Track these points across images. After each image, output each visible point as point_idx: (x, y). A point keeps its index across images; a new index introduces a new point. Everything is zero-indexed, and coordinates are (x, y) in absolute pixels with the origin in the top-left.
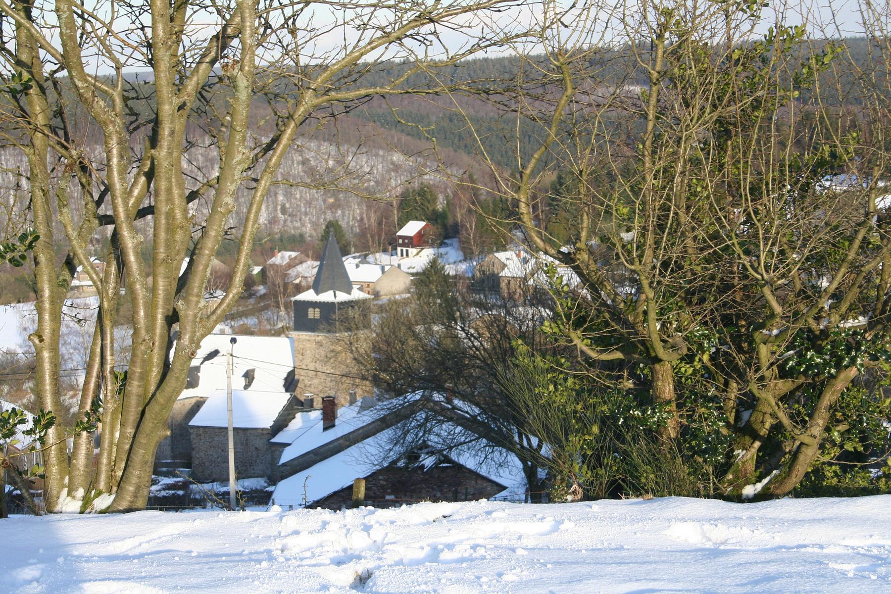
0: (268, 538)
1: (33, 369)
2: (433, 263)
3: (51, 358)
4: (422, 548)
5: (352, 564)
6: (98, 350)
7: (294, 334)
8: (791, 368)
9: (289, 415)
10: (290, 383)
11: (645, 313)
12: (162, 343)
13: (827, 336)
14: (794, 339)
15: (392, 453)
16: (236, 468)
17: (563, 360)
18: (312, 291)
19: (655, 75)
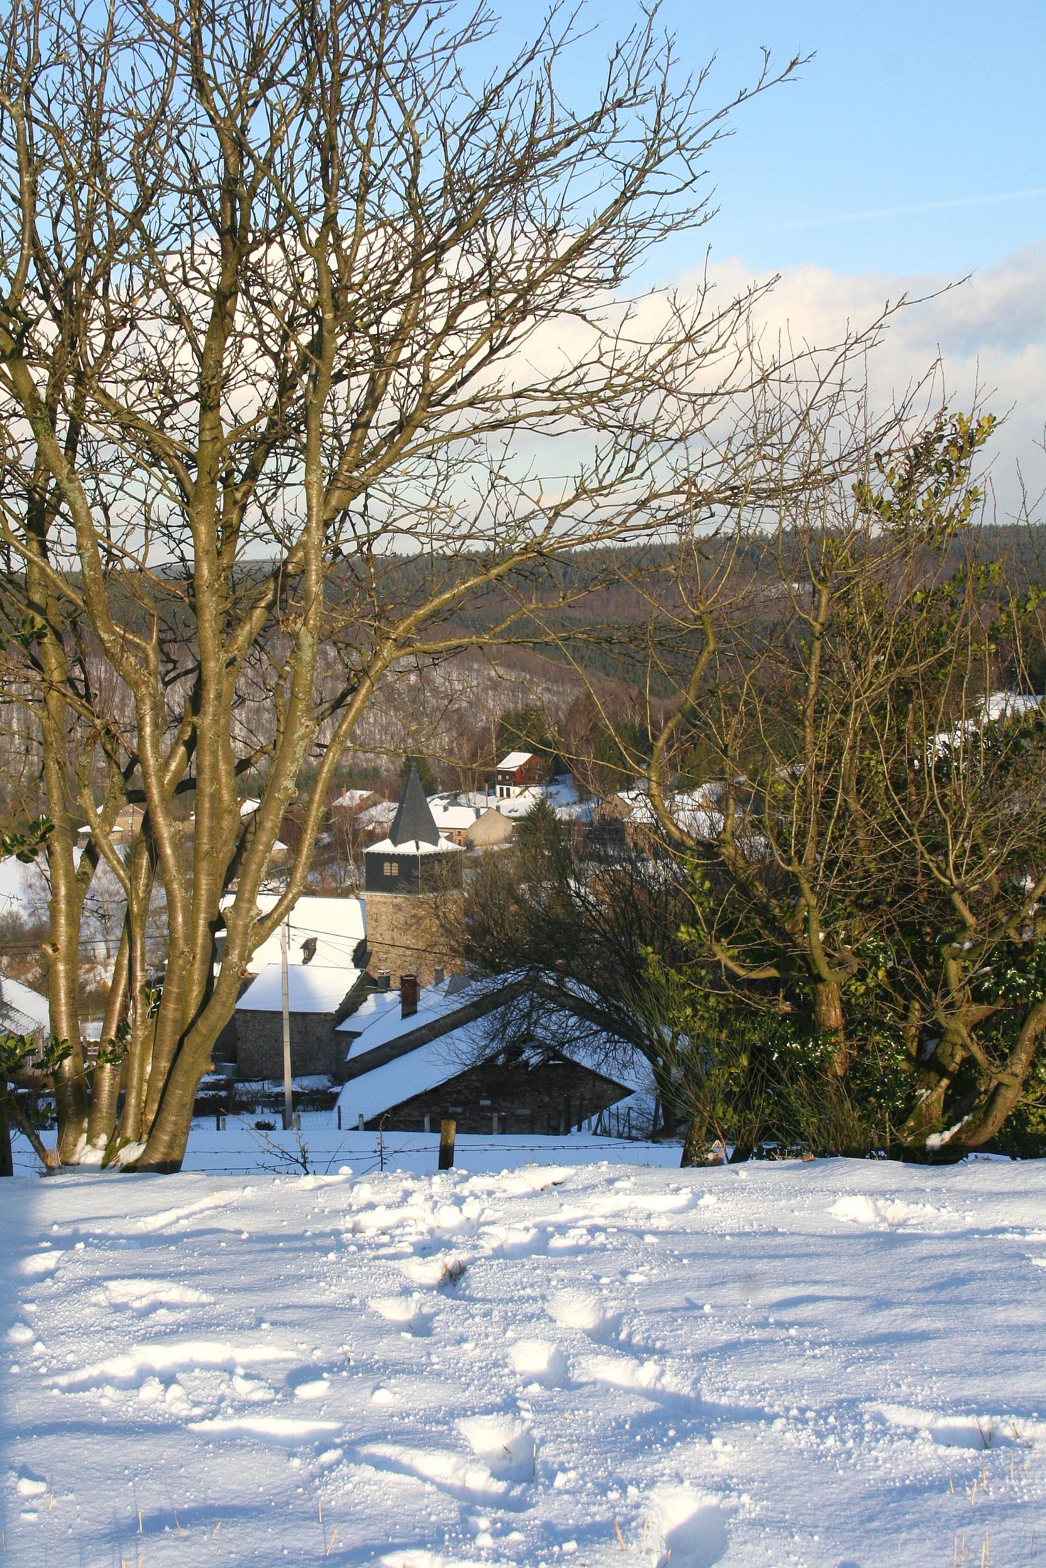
0: (336, 1213)
1: (42, 935)
2: (541, 805)
3: (67, 972)
4: (527, 1229)
5: (440, 1255)
6: (126, 962)
7: (365, 895)
8: (987, 989)
9: (359, 996)
10: (361, 956)
11: (806, 920)
12: (204, 954)
13: (1032, 950)
14: (991, 955)
15: (488, 1051)
16: (293, 1063)
17: (703, 972)
18: (388, 842)
19: (818, 627)
